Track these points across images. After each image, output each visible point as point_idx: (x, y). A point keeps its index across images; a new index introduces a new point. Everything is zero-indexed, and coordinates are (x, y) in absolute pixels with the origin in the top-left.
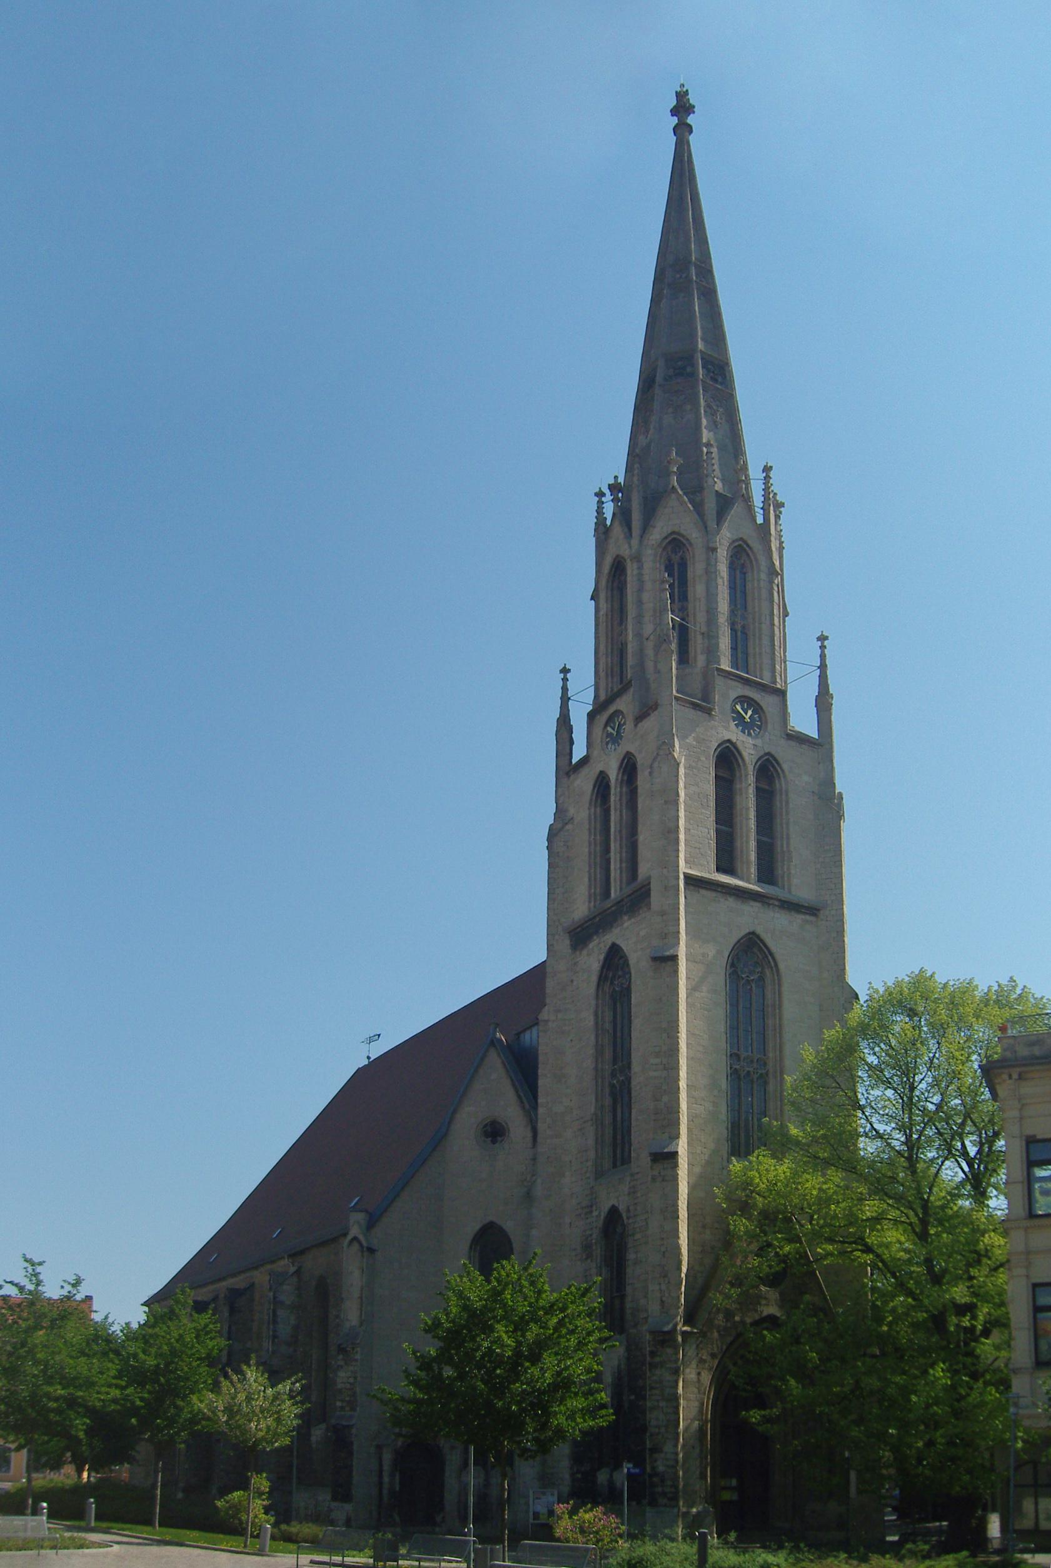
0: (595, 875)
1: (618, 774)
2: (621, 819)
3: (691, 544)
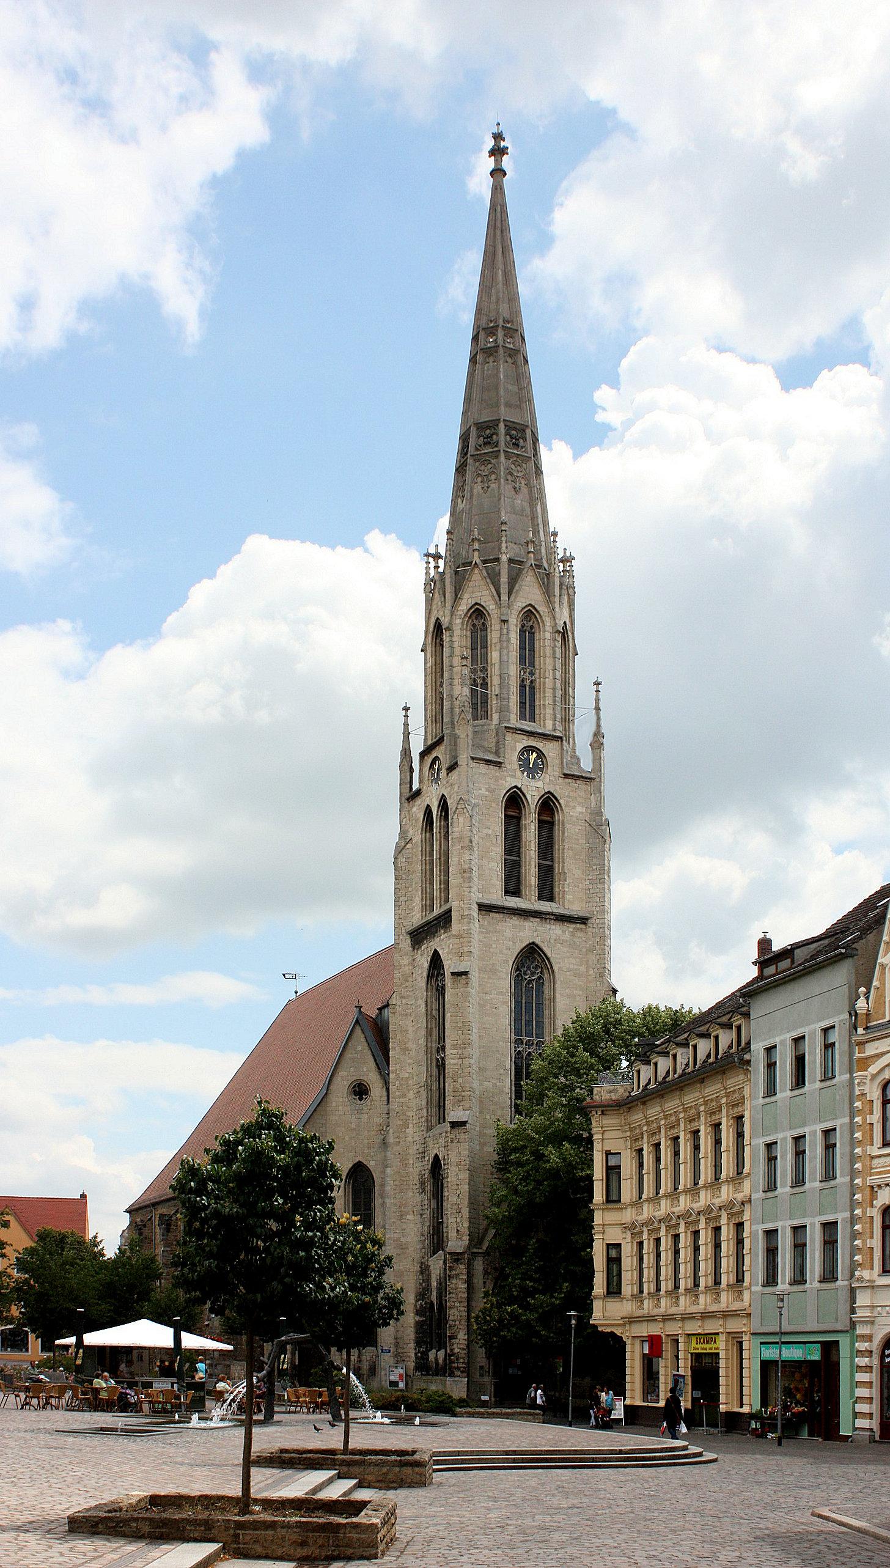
0: (426, 888)
2: (440, 850)
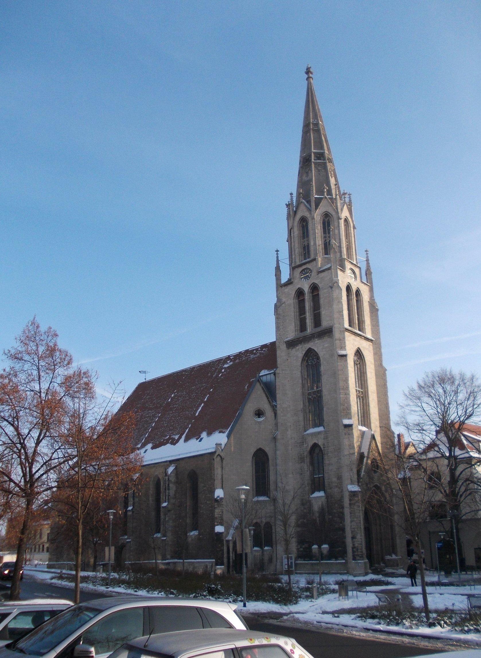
1: (308, 290)
3: (332, 215)
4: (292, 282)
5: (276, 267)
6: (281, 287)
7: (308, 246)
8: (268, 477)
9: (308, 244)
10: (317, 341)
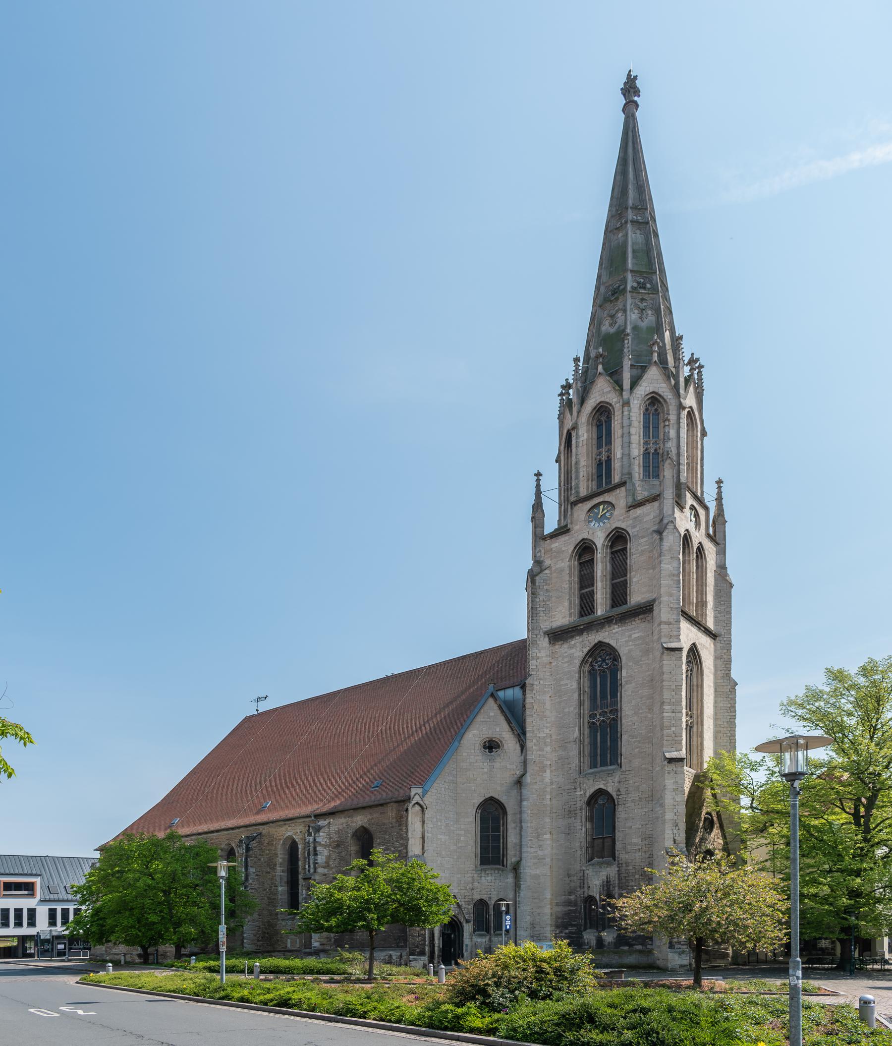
3: (665, 400)
4: (569, 529)
5: (534, 505)
6: (544, 538)
7: (609, 460)
8: (505, 838)
9: (608, 457)
10: (616, 629)
